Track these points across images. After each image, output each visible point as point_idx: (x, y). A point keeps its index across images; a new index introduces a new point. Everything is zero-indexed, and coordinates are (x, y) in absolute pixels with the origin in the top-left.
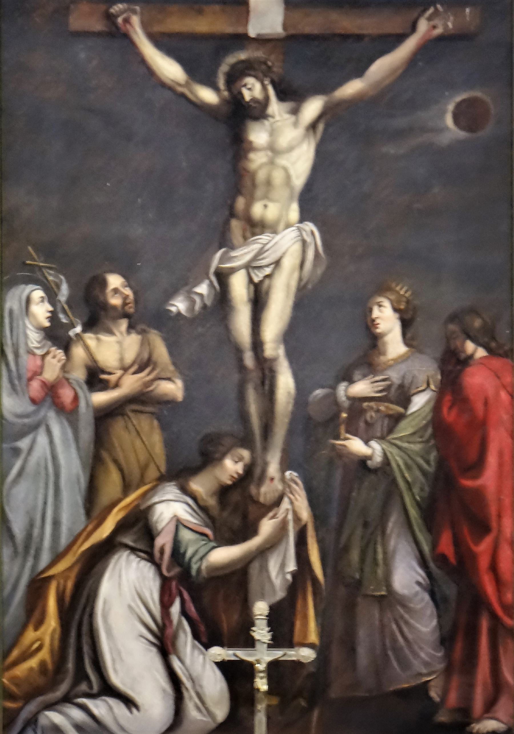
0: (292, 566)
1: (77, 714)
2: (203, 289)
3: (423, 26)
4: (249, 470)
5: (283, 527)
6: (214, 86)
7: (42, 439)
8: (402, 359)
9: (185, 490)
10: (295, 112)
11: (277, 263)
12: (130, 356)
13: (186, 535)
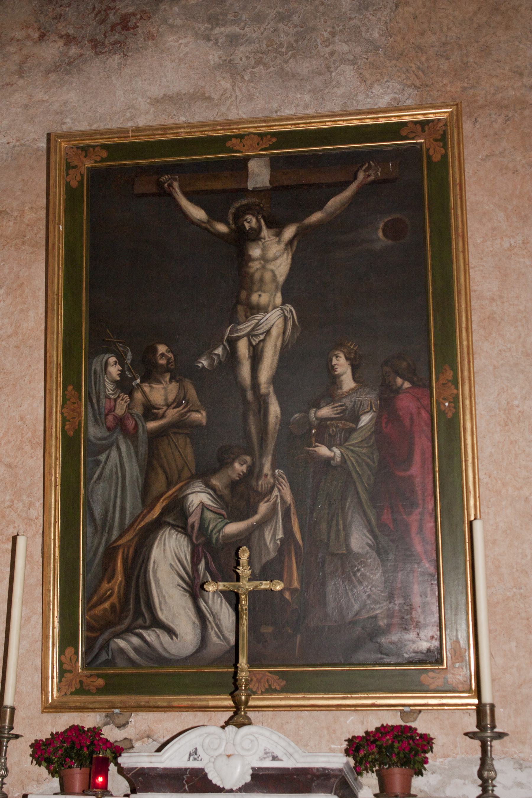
0: (280, 535)
1: (135, 640)
2: (219, 351)
3: (361, 175)
4: (251, 470)
5: (274, 509)
6: (224, 221)
7: (114, 454)
8: (353, 391)
9: (208, 485)
10: (279, 235)
11: (268, 332)
12: (171, 397)
13: (209, 515)
